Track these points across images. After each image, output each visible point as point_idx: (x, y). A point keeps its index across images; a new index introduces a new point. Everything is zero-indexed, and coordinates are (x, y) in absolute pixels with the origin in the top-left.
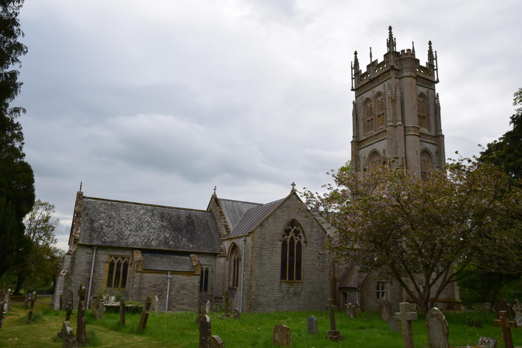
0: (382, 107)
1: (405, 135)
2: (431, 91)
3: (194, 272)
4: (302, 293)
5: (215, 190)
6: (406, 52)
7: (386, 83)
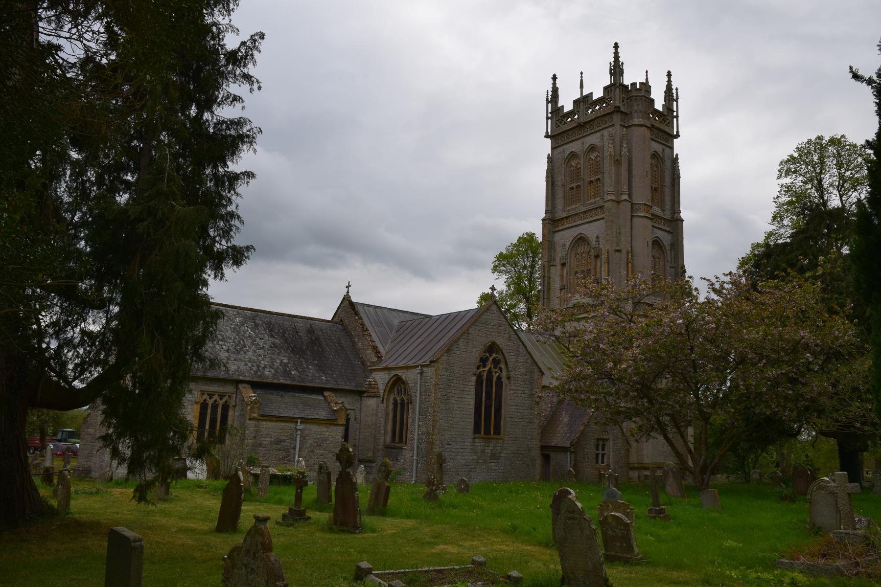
0: (597, 168)
1: (632, 216)
2: (668, 150)
3: (335, 420)
4: (503, 455)
5: (348, 287)
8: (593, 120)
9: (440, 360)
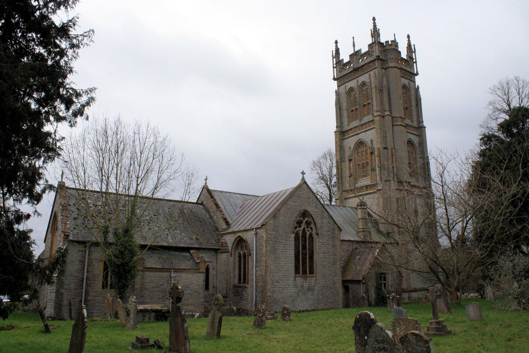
0: (368, 97)
1: (393, 125)
2: (412, 83)
4: (316, 288)
5: (206, 180)
7: (372, 73)
8: (363, 66)
9: (268, 224)
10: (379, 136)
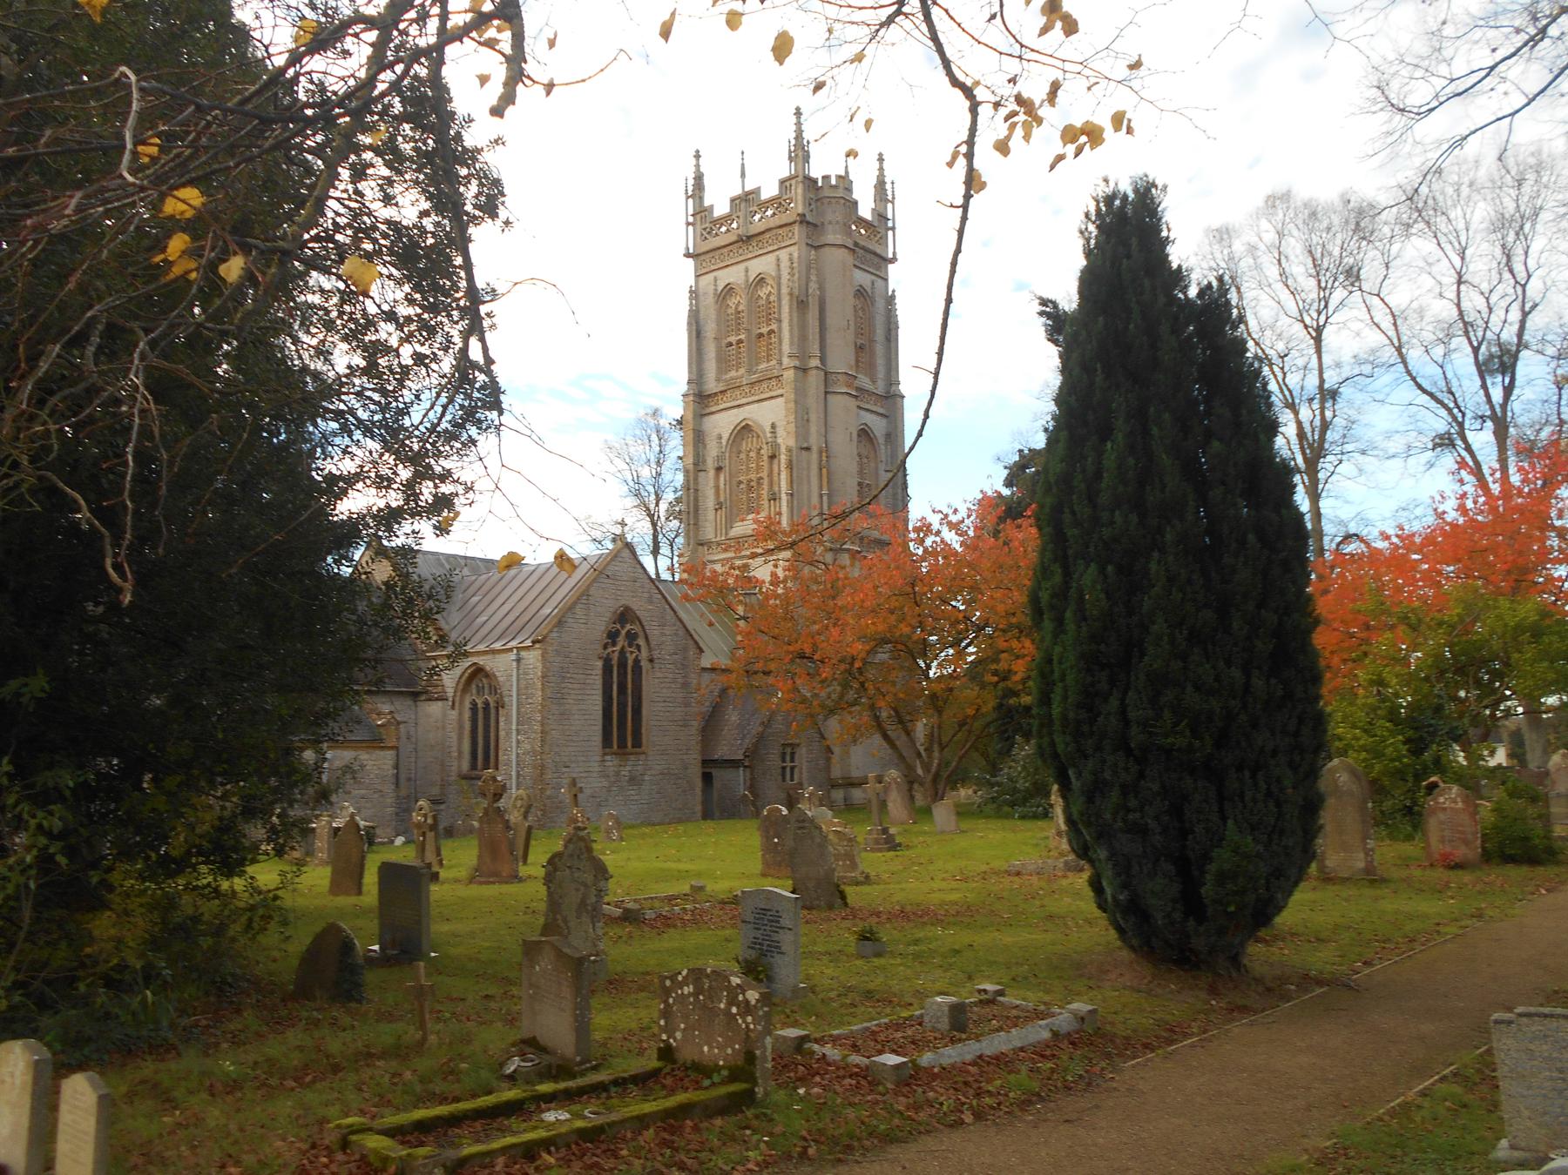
2: (879, 282)
6: (833, 182)
7: (783, 254)
10: (792, 418)
